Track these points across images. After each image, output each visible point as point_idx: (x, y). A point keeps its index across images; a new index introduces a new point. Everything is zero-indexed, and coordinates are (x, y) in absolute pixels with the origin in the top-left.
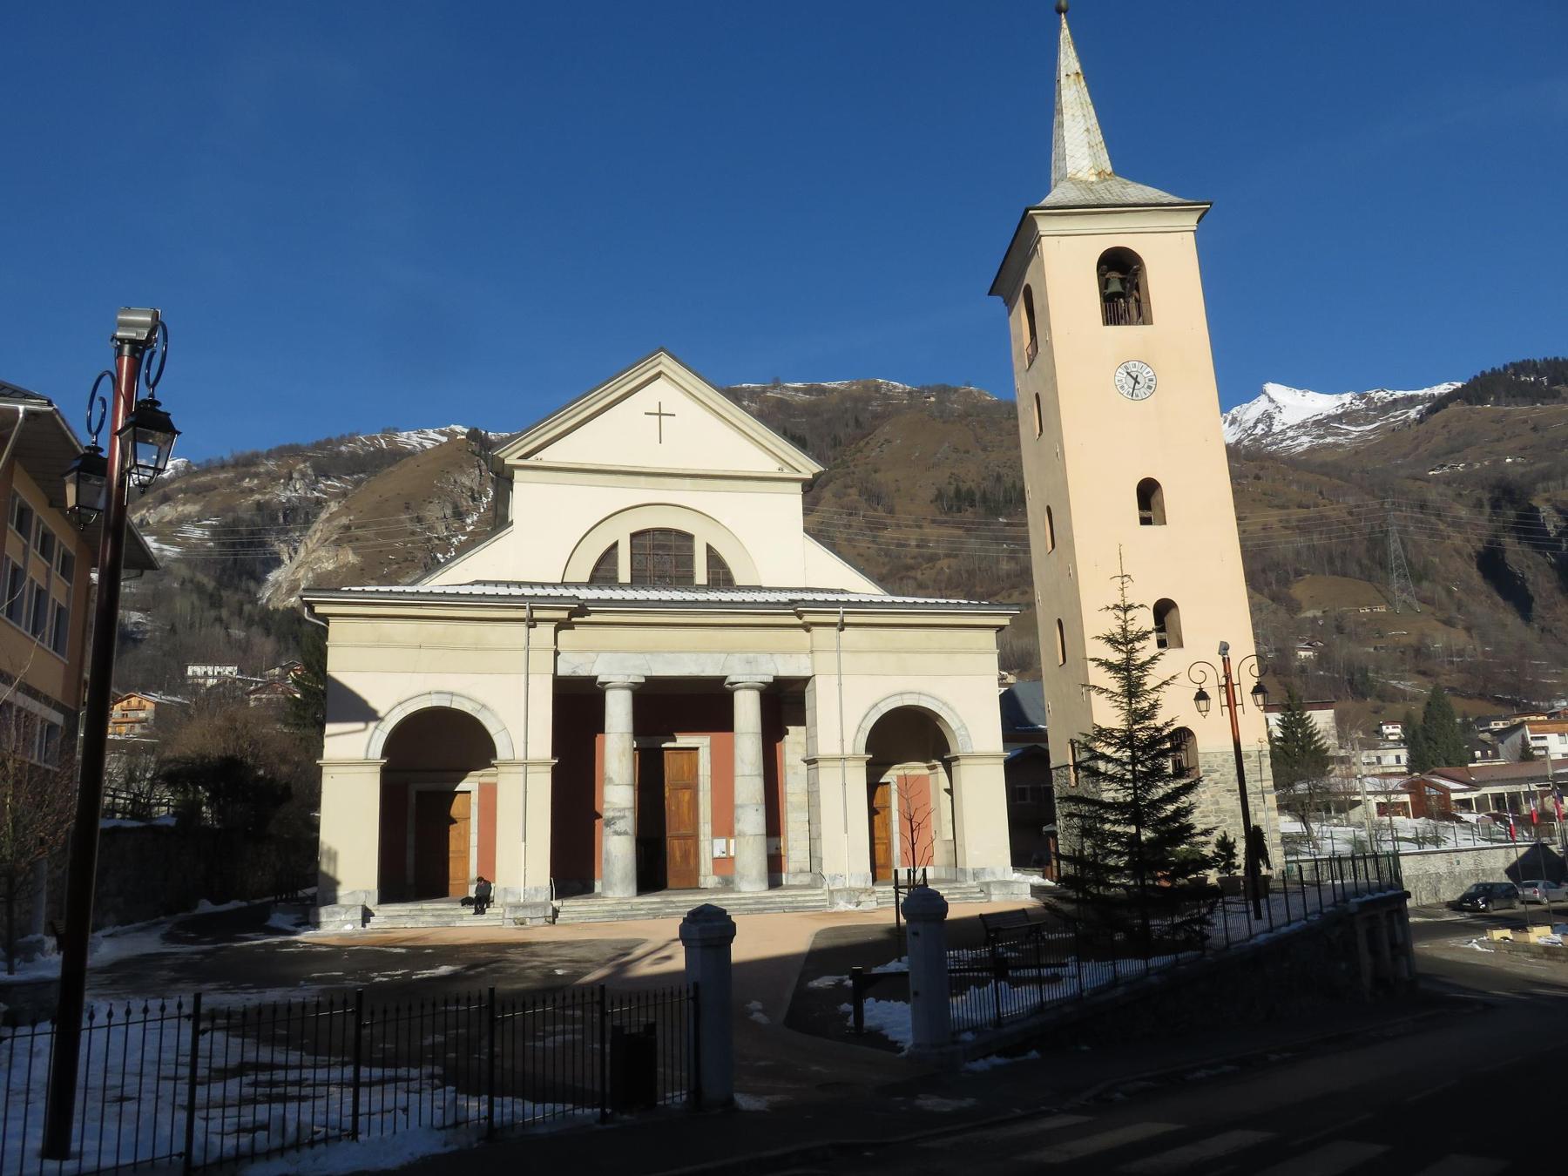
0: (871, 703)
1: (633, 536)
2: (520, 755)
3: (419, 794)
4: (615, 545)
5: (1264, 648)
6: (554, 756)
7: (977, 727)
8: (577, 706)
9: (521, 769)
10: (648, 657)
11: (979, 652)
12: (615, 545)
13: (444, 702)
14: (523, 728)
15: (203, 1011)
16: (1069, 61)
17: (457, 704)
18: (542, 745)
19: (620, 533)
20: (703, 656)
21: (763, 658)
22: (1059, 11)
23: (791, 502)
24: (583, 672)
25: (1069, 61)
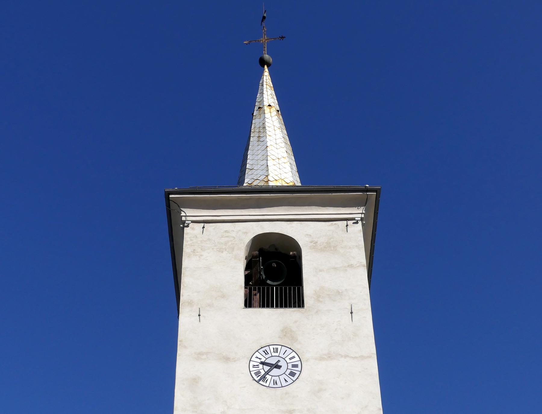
25: (268, 95)
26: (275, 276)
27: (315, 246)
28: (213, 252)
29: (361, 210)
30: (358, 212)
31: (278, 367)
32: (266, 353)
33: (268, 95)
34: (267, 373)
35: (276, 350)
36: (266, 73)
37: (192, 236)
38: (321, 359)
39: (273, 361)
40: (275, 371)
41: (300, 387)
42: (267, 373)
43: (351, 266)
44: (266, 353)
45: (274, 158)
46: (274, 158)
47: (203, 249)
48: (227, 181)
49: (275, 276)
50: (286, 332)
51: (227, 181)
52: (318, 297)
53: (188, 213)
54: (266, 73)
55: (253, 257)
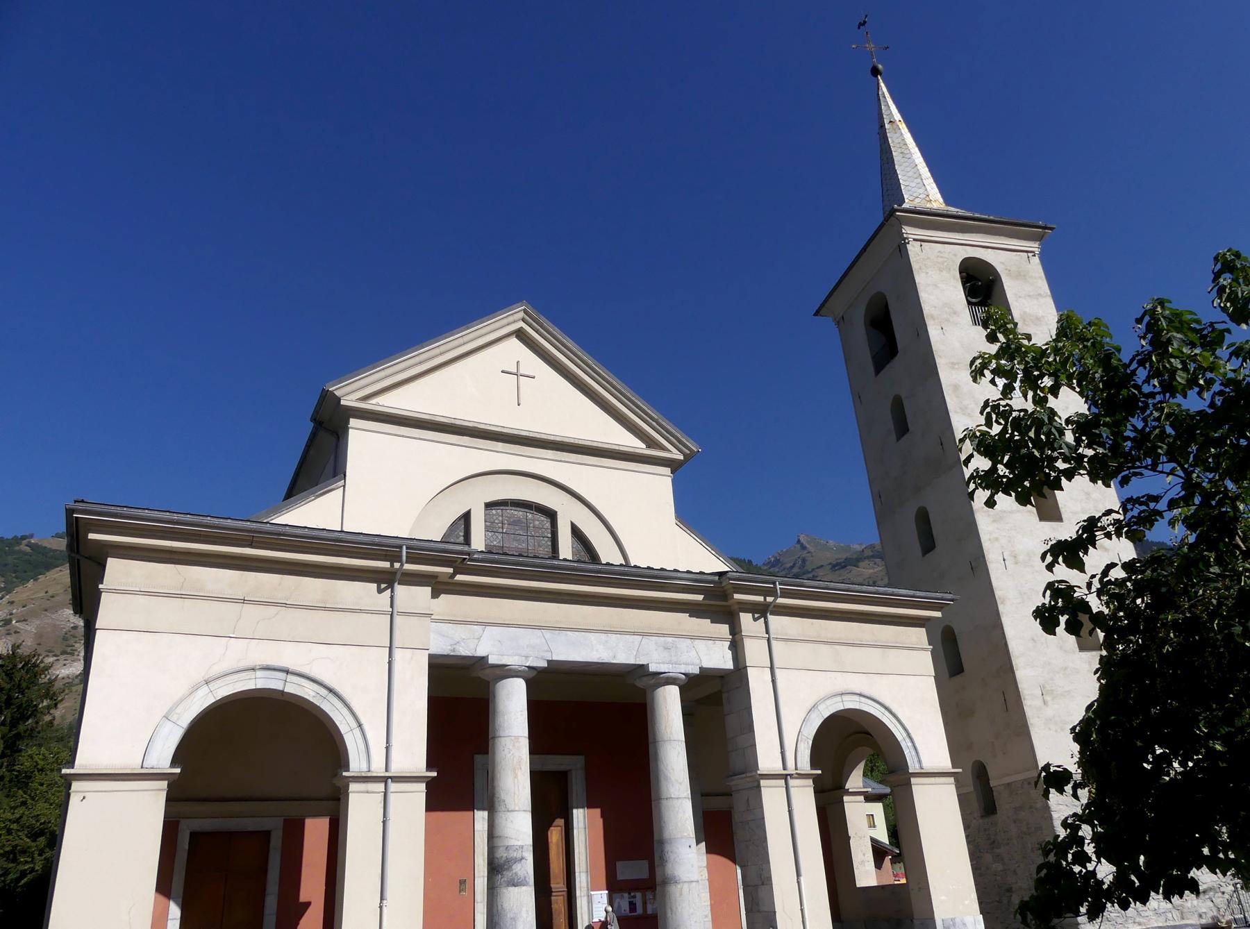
0: (809, 705)
1: (489, 506)
2: (378, 768)
3: (193, 835)
4: (466, 517)
5: (555, 763)
6: (430, 766)
7: (926, 739)
8: (459, 703)
9: (381, 787)
10: (548, 634)
11: (923, 649)
12: (466, 517)
13: (273, 682)
14: (387, 731)
15: (61, 576)
16: (892, 111)
17: (295, 687)
18: (412, 753)
19: (475, 500)
20: (614, 638)
21: (684, 644)
22: (875, 72)
23: (660, 484)
24: (464, 650)
25: (892, 111)
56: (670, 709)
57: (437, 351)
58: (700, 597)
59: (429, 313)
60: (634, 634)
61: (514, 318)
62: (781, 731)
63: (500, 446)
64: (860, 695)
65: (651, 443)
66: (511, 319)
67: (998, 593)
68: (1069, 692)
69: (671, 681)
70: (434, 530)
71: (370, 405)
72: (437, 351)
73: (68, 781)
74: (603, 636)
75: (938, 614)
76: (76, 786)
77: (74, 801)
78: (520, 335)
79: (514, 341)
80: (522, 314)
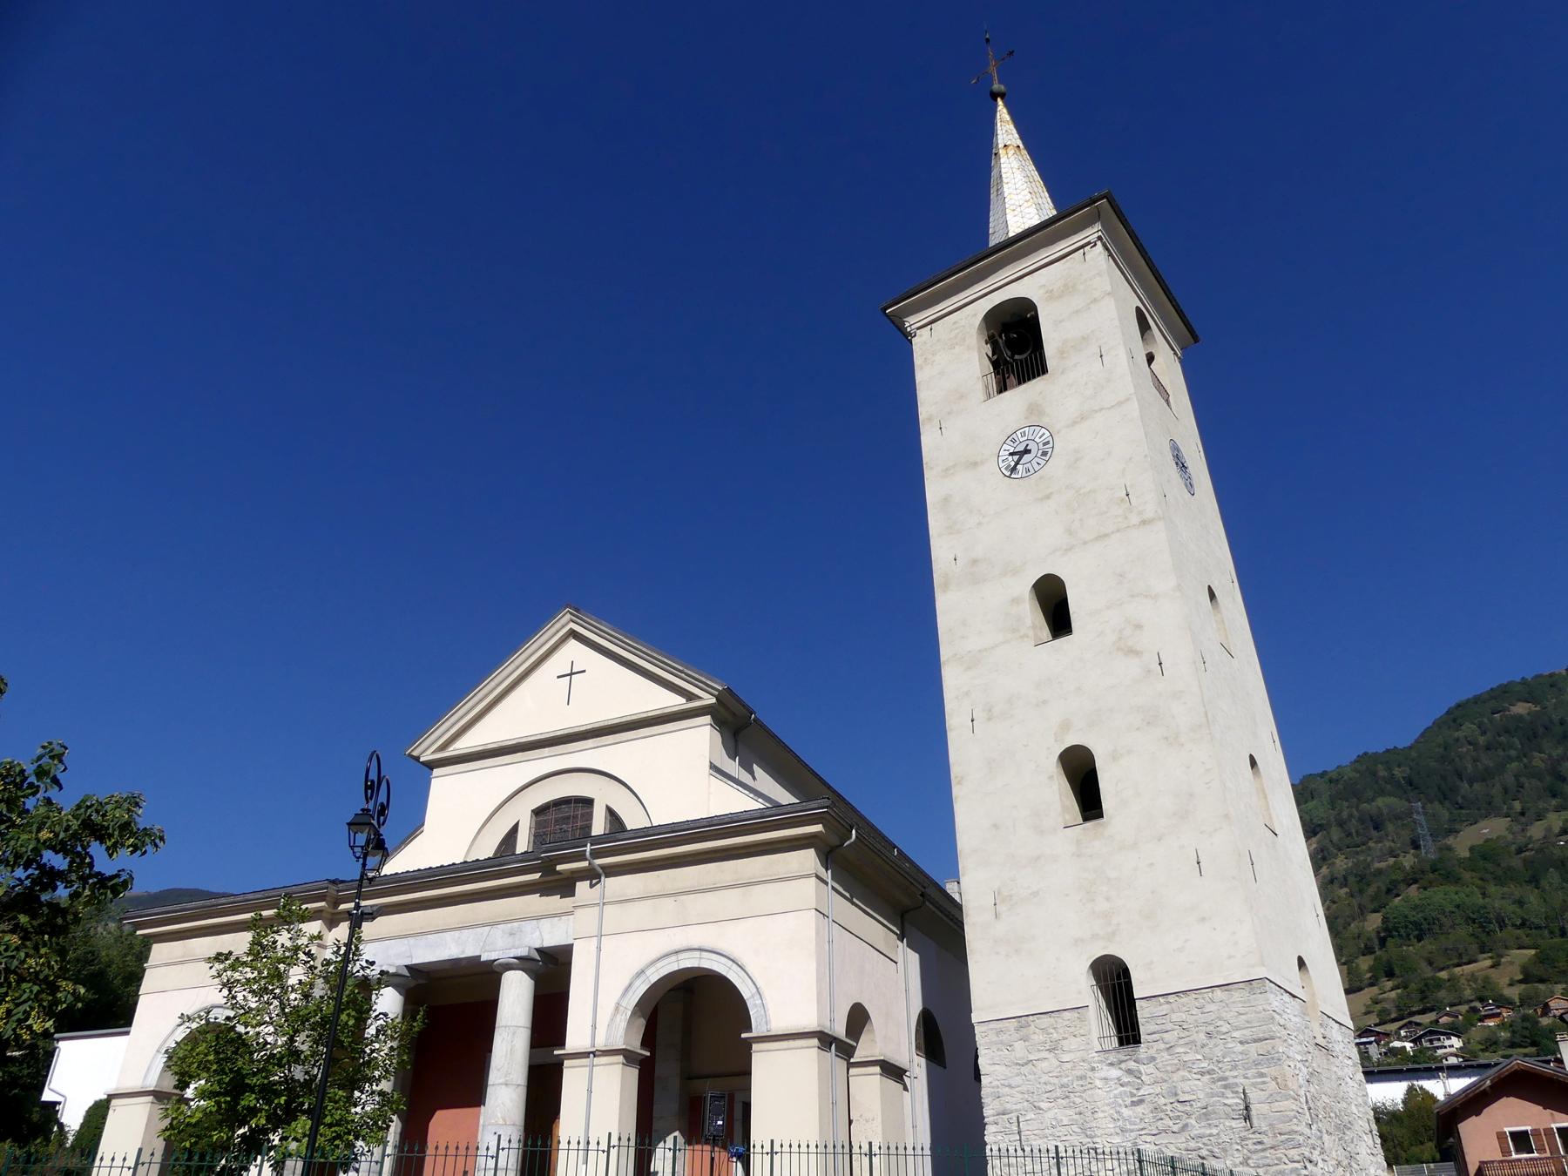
10: (412, 940)
21: (529, 926)
25: (1006, 131)
26: (1017, 346)
27: (1051, 296)
28: (946, 350)
29: (1098, 226)
30: (1093, 232)
31: (1027, 451)
32: (1014, 441)
33: (1006, 131)
34: (1017, 463)
35: (1024, 434)
36: (1002, 112)
37: (920, 343)
38: (1074, 423)
39: (1021, 448)
40: (1026, 458)
41: (1056, 465)
42: (1017, 463)
43: (1095, 301)
44: (1014, 441)
45: (1020, 196)
46: (1020, 196)
47: (934, 354)
48: (968, 248)
49: (1017, 346)
50: (1033, 409)
51: (968, 248)
52: (1062, 353)
53: (912, 322)
54: (1002, 112)
55: (198, 1129)
56: (515, 999)
57: (493, 684)
58: (537, 876)
59: (483, 646)
60: (483, 925)
61: (565, 621)
62: (601, 1012)
63: (546, 751)
64: (701, 950)
65: (690, 697)
66: (558, 626)
67: (955, 771)
68: (1035, 894)
69: (508, 967)
70: (486, 850)
71: (453, 751)
72: (493, 684)
73: (747, 1045)
74: (457, 933)
75: (818, 828)
76: (755, 1047)
77: (755, 1058)
78: (574, 634)
79: (573, 643)
80: (568, 616)
